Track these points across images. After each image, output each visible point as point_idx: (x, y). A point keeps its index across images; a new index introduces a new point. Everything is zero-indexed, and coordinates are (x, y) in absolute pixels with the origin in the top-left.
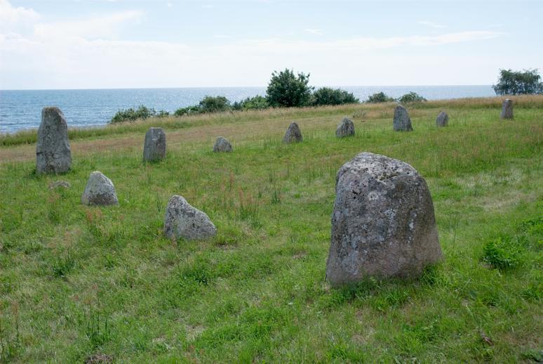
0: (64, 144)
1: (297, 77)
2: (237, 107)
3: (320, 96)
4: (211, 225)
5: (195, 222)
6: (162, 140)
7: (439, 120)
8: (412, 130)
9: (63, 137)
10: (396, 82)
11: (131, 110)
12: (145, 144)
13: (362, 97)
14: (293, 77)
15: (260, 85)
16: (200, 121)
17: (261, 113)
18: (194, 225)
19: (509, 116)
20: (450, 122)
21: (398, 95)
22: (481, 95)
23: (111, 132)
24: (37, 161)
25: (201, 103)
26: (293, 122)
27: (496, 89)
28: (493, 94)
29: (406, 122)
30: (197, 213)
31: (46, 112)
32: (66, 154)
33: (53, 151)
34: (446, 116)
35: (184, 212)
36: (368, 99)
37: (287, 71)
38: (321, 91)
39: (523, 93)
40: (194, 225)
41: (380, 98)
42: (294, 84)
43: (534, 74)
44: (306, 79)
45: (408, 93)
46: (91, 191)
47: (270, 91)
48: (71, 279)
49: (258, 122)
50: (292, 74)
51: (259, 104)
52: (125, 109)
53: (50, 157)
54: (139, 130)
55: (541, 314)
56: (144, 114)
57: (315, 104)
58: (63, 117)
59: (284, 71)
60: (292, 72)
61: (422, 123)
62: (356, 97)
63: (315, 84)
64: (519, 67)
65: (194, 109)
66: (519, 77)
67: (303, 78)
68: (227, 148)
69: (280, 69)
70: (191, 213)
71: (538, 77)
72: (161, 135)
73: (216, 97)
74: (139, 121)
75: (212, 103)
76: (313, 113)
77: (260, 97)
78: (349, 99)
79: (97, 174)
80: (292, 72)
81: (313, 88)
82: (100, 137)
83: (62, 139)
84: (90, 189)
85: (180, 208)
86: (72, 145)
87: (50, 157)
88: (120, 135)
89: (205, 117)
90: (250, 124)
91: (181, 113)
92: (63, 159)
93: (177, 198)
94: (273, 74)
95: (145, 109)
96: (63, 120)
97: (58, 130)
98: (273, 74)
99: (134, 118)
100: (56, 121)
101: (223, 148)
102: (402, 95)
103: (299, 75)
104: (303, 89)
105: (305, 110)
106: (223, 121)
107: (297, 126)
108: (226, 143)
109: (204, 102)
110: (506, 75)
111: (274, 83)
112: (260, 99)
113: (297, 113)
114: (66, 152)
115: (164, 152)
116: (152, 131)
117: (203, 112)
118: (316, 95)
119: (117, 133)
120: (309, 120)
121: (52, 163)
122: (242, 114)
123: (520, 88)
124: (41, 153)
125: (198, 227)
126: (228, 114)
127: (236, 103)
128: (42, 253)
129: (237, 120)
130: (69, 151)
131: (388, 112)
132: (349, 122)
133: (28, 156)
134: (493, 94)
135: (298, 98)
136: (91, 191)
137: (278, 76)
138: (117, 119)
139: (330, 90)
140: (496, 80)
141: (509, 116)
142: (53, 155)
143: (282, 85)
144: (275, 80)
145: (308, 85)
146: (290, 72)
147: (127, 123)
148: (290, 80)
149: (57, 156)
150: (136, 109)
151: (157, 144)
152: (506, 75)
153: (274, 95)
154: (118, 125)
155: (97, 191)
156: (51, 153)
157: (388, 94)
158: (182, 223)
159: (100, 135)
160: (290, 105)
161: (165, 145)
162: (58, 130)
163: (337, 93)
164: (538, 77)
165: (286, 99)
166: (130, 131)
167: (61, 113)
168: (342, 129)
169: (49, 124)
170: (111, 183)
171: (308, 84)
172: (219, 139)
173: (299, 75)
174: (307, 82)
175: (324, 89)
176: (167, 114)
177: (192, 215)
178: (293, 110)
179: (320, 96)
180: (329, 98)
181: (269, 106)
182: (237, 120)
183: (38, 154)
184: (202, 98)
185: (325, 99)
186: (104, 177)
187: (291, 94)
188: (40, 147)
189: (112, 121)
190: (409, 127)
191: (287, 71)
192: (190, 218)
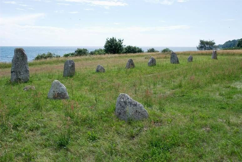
0: (26, 67)
1: (117, 41)
2: (92, 53)
3: (128, 49)
4: (146, 111)
5: (137, 109)
6: (73, 66)
7: (189, 59)
8: (179, 63)
9: (26, 63)
10: (160, 44)
11: (44, 54)
12: (64, 68)
13: (145, 50)
14: (116, 41)
15: (101, 45)
16: (76, 60)
17: (103, 56)
18: (137, 111)
19: (215, 58)
20: (194, 60)
21: (160, 50)
22: (192, 50)
23: (36, 64)
24: (11, 76)
25: (76, 52)
26: (130, 58)
27: (198, 48)
28: (196, 50)
29: (176, 59)
30: (138, 104)
31: (17, 51)
32: (27, 72)
33: (20, 70)
34: (192, 57)
35: (131, 103)
36: (147, 51)
37: (113, 38)
38: (128, 47)
39: (209, 49)
40: (137, 111)
41: (152, 50)
42: (116, 44)
43: (213, 42)
44: (122, 42)
45: (165, 48)
46: (54, 91)
47: (105, 47)
48: (72, 150)
49: (102, 60)
50: (115, 40)
51: (101, 52)
52: (41, 53)
53: (18, 74)
54: (49, 63)
55: (241, 144)
56: (50, 56)
57: (126, 53)
58: (25, 53)
59: (112, 38)
60: (115, 38)
61: (183, 61)
62: (143, 50)
63: (126, 44)
64: (207, 39)
65: (72, 54)
66: (207, 43)
67: (120, 41)
68: (102, 71)
69: (110, 37)
70: (135, 104)
71: (214, 43)
72: (73, 63)
73: (82, 49)
74: (48, 59)
75: (81, 52)
76: (138, 56)
77: (101, 49)
78: (140, 51)
79: (57, 82)
80: (115, 38)
81: (125, 46)
82: (31, 66)
83: (25, 65)
84: (53, 90)
85: (127, 101)
86: (29, 68)
87: (18, 74)
88: (40, 65)
89: (78, 58)
90: (99, 61)
91: (66, 56)
92: (25, 75)
93: (124, 95)
94: (107, 39)
95: (50, 54)
96: (26, 55)
97: (23, 60)
98: (107, 39)
99: (46, 58)
100: (22, 55)
101: (99, 70)
102: (163, 49)
103: (119, 40)
104: (121, 46)
105: (122, 55)
106: (87, 59)
107: (132, 60)
108: (102, 68)
109: (77, 51)
110: (202, 42)
111: (107, 43)
112: (101, 50)
113: (119, 56)
114: (27, 71)
115: (74, 72)
116: (68, 62)
117: (76, 56)
118: (126, 49)
119: (38, 64)
120: (122, 59)
121: (19, 77)
122: (95, 56)
123: (207, 47)
124: (14, 71)
125: (139, 112)
126: (87, 57)
127: (91, 52)
128: (42, 130)
129: (93, 59)
130: (28, 71)
131: (169, 56)
132: (154, 59)
133: (7, 74)
134: (196, 50)
135: (118, 50)
136: (54, 91)
137: (109, 40)
138: (38, 58)
139: (132, 47)
140: (198, 44)
141: (215, 58)
142: (20, 73)
143: (111, 44)
144: (108, 42)
145: (123, 44)
146: (114, 39)
147: (43, 60)
148: (115, 42)
149: (22, 73)
150: (46, 54)
151: (71, 68)
152: (202, 42)
153: (108, 49)
154: (38, 61)
155: (57, 91)
156: (19, 71)
157: (156, 49)
158: (129, 109)
159: (31, 65)
160: (114, 53)
161: (74, 68)
162: (23, 60)
163: (135, 48)
164: (214, 43)
165: (113, 50)
166: (45, 63)
167: (24, 51)
168: (151, 62)
169: (18, 56)
170: (65, 87)
171: (122, 44)
172: (98, 66)
173: (119, 40)
174: (122, 43)
175: (129, 46)
176: (60, 56)
177: (135, 105)
178: (117, 55)
179: (128, 49)
180: (131, 50)
181: (106, 53)
182: (93, 59)
183: (12, 72)
184: (76, 49)
185: (130, 50)
186: (61, 84)
187: (115, 48)
188: (13, 68)
189: (35, 59)
190: (178, 62)
191: (113, 38)
192: (134, 107)
